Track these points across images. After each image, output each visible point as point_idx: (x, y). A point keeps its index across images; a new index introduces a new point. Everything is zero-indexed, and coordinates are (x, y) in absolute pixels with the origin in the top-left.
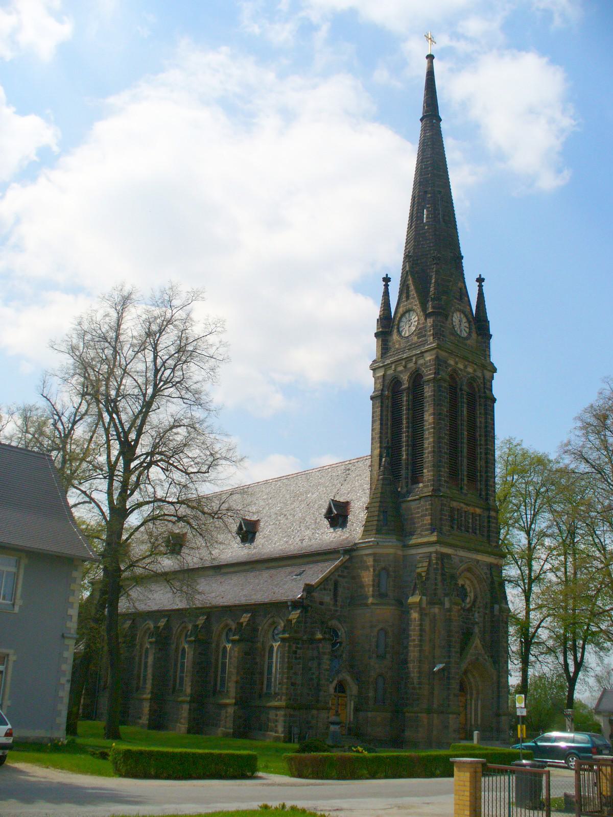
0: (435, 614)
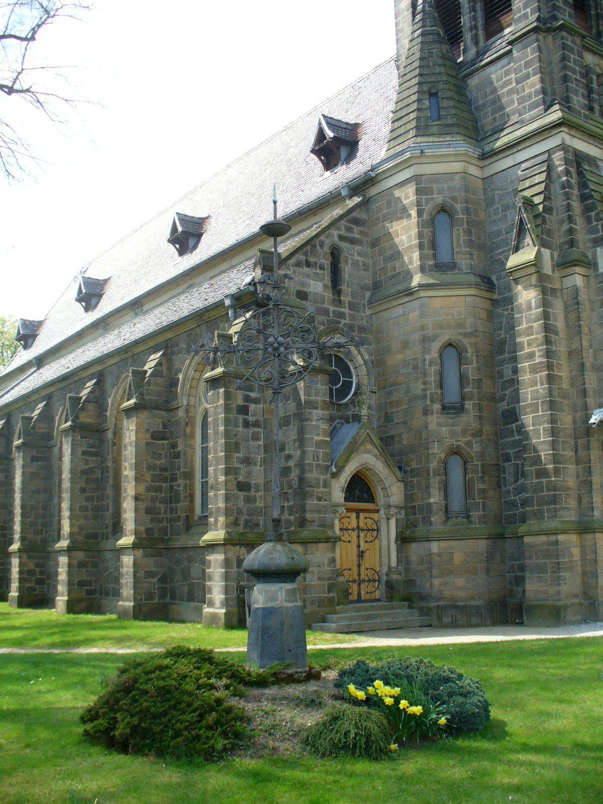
0: (576, 290)
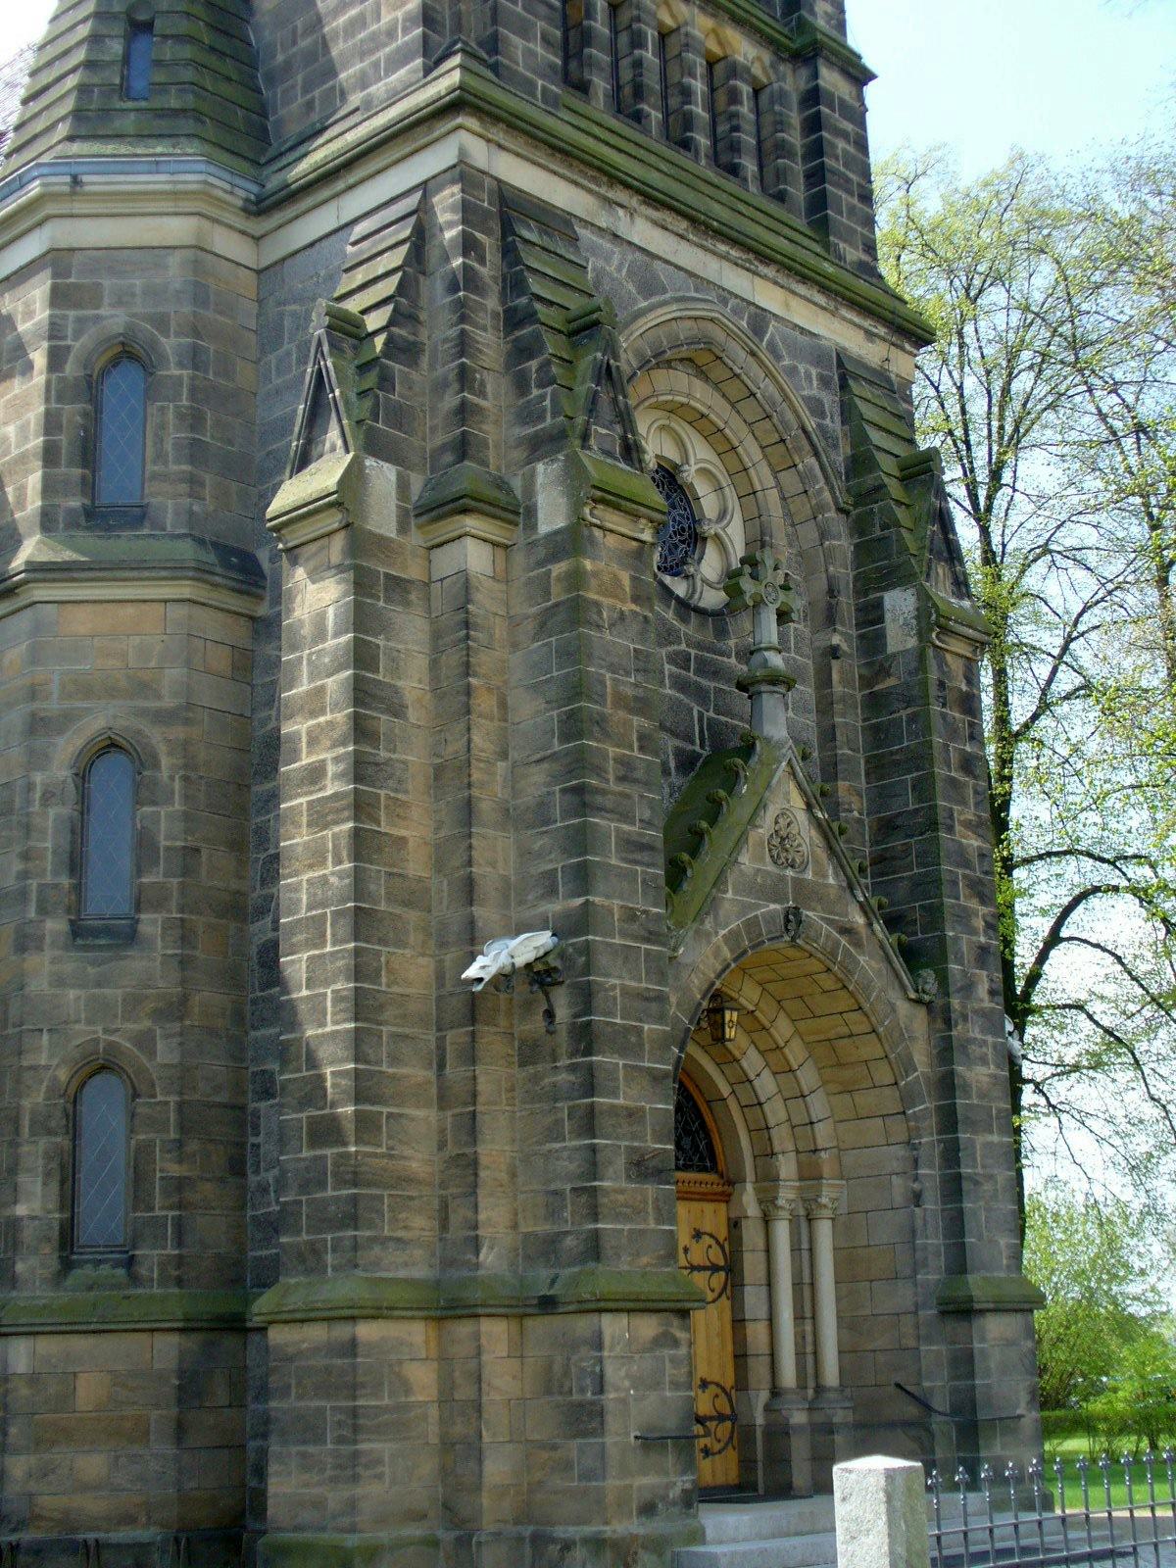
0: (466, 585)
